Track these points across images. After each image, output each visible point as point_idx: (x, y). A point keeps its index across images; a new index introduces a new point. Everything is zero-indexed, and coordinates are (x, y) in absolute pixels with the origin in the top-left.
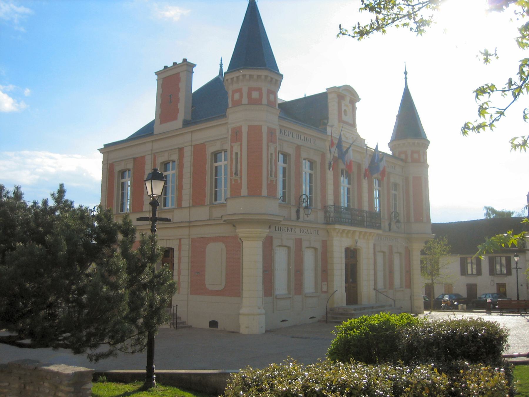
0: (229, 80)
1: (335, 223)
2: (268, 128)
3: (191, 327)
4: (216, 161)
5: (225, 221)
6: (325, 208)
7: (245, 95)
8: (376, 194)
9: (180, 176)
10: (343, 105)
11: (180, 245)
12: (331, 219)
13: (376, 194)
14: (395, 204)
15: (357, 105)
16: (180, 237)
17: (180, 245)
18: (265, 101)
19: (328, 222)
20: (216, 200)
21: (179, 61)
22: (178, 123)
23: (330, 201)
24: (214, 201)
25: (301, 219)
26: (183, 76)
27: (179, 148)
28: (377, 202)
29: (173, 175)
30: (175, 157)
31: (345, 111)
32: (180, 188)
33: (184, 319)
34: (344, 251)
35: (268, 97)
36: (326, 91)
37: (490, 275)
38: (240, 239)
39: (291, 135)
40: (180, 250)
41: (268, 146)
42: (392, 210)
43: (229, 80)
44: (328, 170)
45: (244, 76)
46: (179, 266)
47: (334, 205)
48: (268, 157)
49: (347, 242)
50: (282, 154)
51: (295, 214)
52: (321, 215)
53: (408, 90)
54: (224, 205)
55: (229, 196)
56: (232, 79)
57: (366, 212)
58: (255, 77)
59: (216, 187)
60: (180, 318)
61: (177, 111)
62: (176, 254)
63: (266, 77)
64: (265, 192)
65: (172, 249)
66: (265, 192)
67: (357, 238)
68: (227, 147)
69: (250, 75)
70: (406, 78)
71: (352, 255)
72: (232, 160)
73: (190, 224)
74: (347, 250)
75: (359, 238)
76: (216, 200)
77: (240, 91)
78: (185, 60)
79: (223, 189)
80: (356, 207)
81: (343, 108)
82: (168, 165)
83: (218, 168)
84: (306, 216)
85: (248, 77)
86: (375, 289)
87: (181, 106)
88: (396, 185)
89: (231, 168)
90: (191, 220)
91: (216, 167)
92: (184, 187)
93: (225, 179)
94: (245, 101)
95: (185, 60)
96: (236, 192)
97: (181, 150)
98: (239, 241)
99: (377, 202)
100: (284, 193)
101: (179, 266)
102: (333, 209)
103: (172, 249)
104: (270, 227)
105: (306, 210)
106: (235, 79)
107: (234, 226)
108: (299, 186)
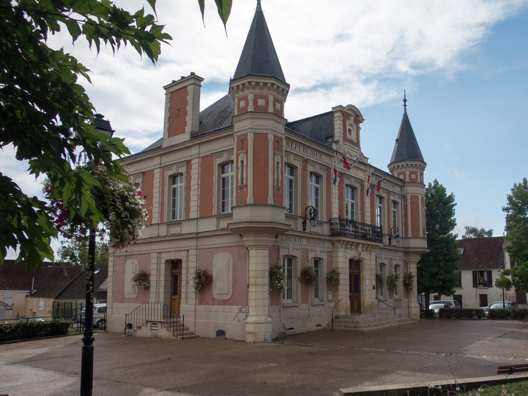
0: (235, 88)
1: (339, 235)
2: (275, 136)
3: (198, 337)
4: (223, 172)
5: (231, 230)
6: (330, 222)
7: (251, 103)
8: (377, 211)
9: (188, 189)
10: (348, 124)
11: (188, 257)
12: (336, 231)
13: (377, 211)
14: (395, 221)
15: (361, 125)
16: (187, 248)
17: (188, 257)
18: (271, 109)
19: (334, 234)
20: (223, 211)
21: (187, 74)
22: (185, 137)
23: (335, 215)
24: (221, 212)
25: (307, 230)
26: (190, 89)
27: (186, 161)
28: (378, 219)
29: (181, 187)
30: (183, 170)
31: (350, 130)
32: (188, 200)
33: (192, 329)
34: (348, 261)
35: (274, 105)
36: (331, 110)
37: (474, 287)
38: (247, 248)
39: (297, 148)
40: (188, 261)
41: (274, 154)
42: (392, 225)
43: (235, 88)
44: (334, 185)
45: (250, 83)
47: (339, 218)
48: (274, 164)
49: (352, 253)
50: (289, 166)
51: (302, 225)
52: (325, 230)
53: (407, 116)
54: (230, 215)
55: (234, 204)
56: (238, 86)
57: (369, 226)
58: (261, 84)
59: (223, 198)
60: (188, 329)
61: (185, 124)
62: (184, 265)
63: (273, 84)
64: (270, 201)
65: (180, 261)
66: (270, 201)
67: (360, 249)
68: (234, 158)
69: (256, 82)
70: (405, 105)
71: (355, 264)
72: (237, 168)
73: (198, 236)
74: (351, 261)
75: (363, 251)
76: (223, 211)
77: (246, 98)
78: (193, 74)
79: (230, 200)
80: (359, 221)
81: (348, 127)
82: (176, 178)
83: (226, 179)
84: (312, 227)
85: (253, 83)
86: (377, 298)
87: (189, 119)
88: (395, 203)
89: (237, 177)
90: (199, 231)
91: (224, 179)
92: (192, 199)
93: (232, 189)
94: (251, 108)
95: (193, 74)
96: (241, 204)
97: (188, 162)
98: (246, 250)
99: (378, 219)
100: (291, 204)
101: (187, 277)
102: (338, 222)
103: (180, 261)
104: (276, 237)
105: (313, 222)
106: (241, 86)
107: (241, 235)
108: (305, 197)
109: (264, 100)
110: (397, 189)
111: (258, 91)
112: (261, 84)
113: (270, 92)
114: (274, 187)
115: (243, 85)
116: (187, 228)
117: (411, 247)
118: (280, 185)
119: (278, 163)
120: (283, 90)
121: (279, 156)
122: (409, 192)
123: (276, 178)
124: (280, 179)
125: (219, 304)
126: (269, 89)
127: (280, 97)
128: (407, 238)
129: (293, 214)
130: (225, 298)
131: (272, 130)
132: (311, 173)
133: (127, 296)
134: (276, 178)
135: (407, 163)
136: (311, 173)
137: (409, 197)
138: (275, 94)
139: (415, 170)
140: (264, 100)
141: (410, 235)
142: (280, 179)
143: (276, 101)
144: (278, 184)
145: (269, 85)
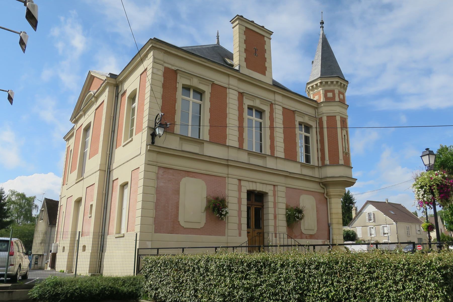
2: (341, 117)
18: (337, 99)
46: (240, 194)
63: (337, 82)
64: (341, 162)
66: (341, 162)
101: (240, 194)
109: (331, 93)
110: (311, 111)
111: (327, 88)
112: (329, 83)
113: (336, 87)
114: (343, 152)
115: (317, 85)
116: (271, 163)
117: (328, 176)
118: (347, 151)
119: (344, 136)
120: (344, 85)
121: (345, 131)
122: (324, 112)
123: (344, 146)
124: (347, 147)
125: (306, 238)
126: (335, 85)
127: (342, 90)
128: (324, 165)
129: (311, 164)
130: (311, 233)
131: (339, 113)
132: (300, 124)
133: (182, 224)
134: (344, 146)
135: (322, 81)
136: (300, 124)
137: (325, 119)
138: (339, 88)
139: (332, 88)
140: (331, 93)
141: (327, 162)
142: (347, 147)
143: (340, 93)
144: (345, 150)
145: (335, 82)
